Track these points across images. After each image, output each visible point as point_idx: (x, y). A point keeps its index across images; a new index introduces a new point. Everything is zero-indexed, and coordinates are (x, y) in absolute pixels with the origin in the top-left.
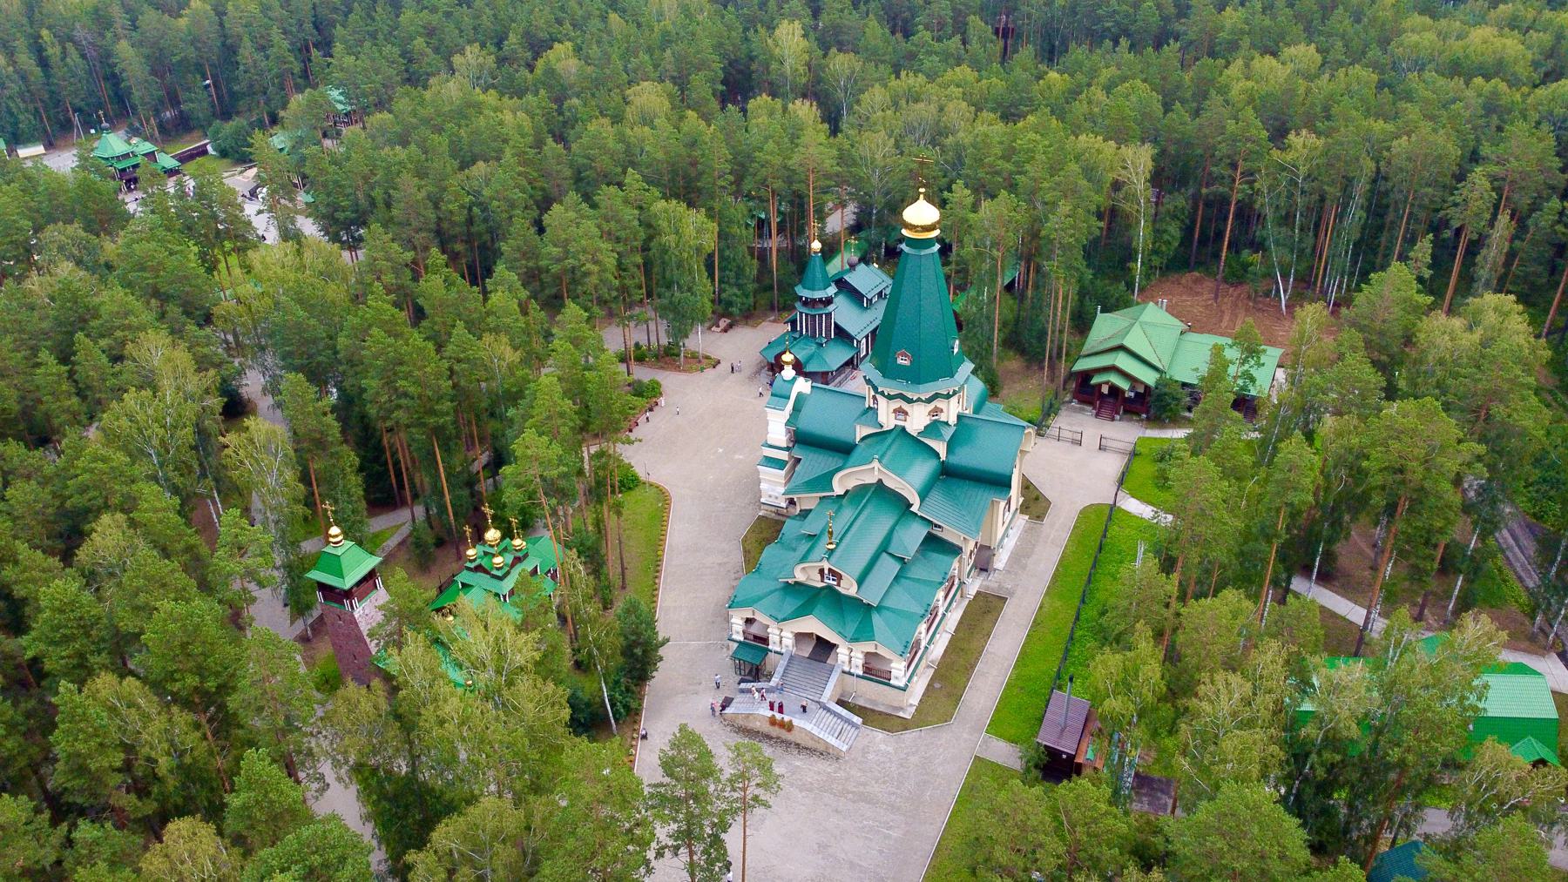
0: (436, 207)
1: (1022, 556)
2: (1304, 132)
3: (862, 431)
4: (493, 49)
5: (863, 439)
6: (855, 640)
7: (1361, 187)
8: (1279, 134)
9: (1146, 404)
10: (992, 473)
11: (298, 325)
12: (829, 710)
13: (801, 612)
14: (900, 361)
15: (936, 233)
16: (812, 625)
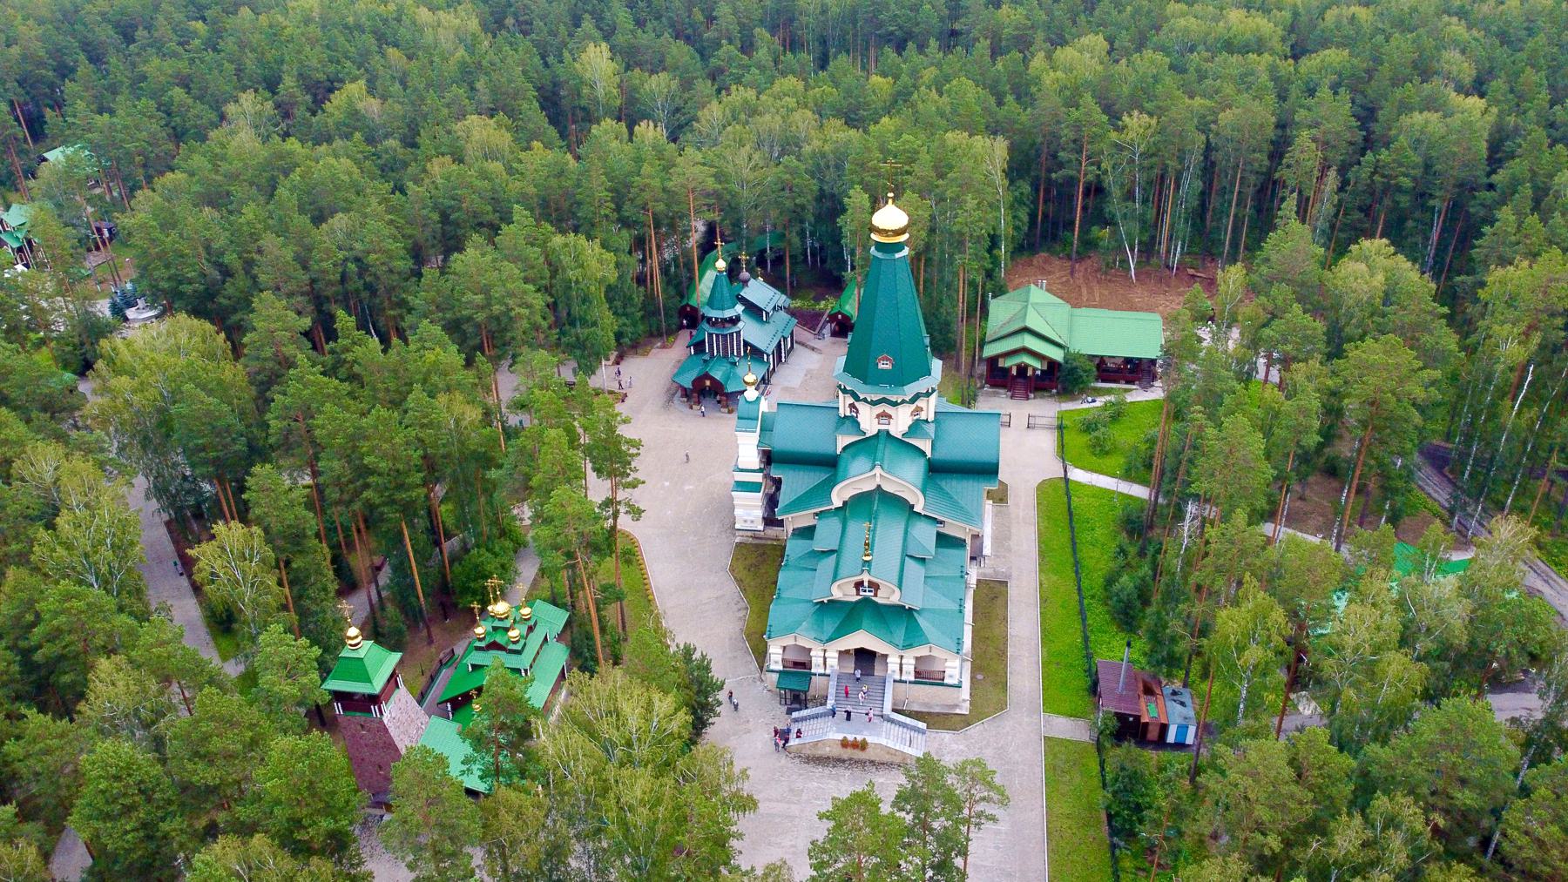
0: (305, 268)
1: (1010, 539)
2: (1136, 113)
3: (843, 441)
4: (268, 94)
5: (844, 449)
6: (905, 647)
7: (1195, 159)
8: (1113, 114)
9: (1056, 379)
10: (953, 462)
11: (208, 413)
12: (892, 721)
13: (840, 632)
14: (881, 366)
15: (905, 237)
16: (861, 639)
